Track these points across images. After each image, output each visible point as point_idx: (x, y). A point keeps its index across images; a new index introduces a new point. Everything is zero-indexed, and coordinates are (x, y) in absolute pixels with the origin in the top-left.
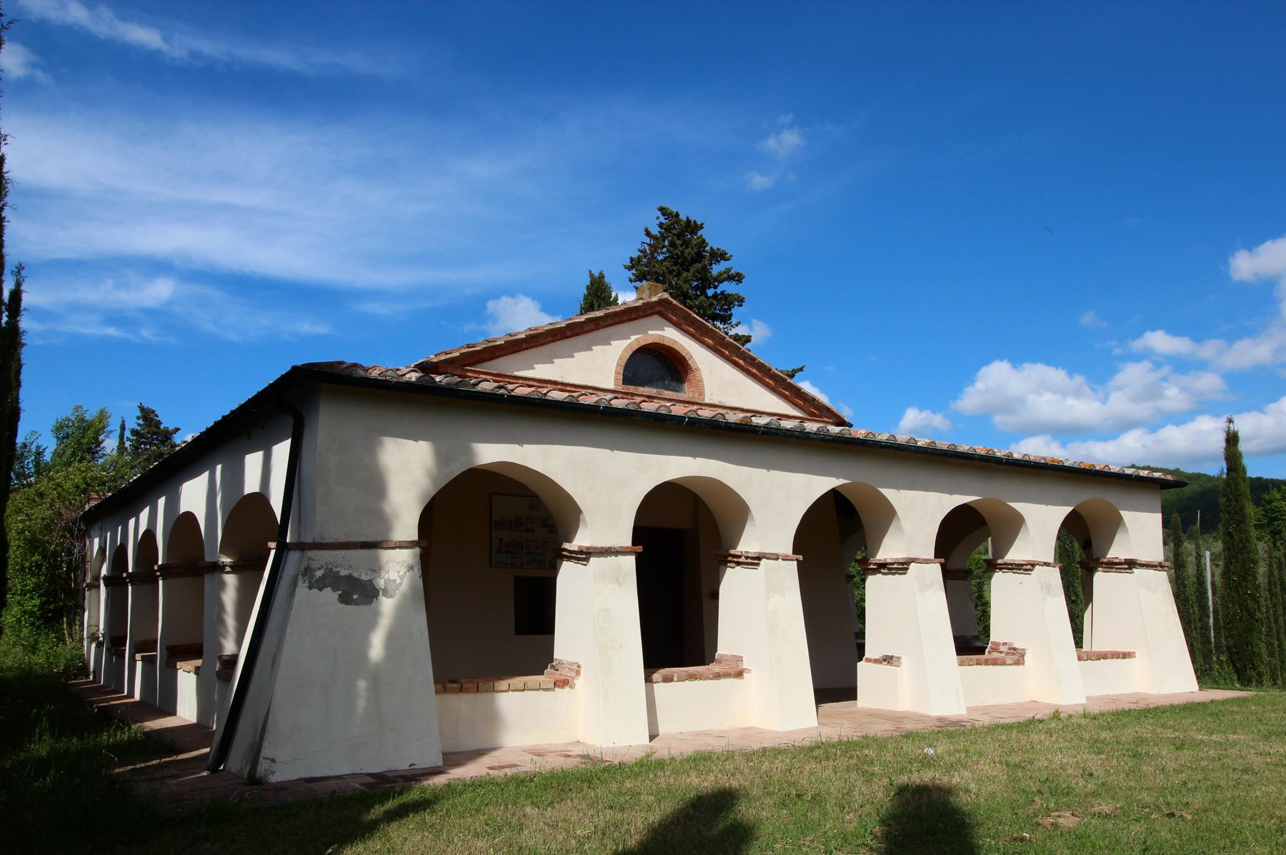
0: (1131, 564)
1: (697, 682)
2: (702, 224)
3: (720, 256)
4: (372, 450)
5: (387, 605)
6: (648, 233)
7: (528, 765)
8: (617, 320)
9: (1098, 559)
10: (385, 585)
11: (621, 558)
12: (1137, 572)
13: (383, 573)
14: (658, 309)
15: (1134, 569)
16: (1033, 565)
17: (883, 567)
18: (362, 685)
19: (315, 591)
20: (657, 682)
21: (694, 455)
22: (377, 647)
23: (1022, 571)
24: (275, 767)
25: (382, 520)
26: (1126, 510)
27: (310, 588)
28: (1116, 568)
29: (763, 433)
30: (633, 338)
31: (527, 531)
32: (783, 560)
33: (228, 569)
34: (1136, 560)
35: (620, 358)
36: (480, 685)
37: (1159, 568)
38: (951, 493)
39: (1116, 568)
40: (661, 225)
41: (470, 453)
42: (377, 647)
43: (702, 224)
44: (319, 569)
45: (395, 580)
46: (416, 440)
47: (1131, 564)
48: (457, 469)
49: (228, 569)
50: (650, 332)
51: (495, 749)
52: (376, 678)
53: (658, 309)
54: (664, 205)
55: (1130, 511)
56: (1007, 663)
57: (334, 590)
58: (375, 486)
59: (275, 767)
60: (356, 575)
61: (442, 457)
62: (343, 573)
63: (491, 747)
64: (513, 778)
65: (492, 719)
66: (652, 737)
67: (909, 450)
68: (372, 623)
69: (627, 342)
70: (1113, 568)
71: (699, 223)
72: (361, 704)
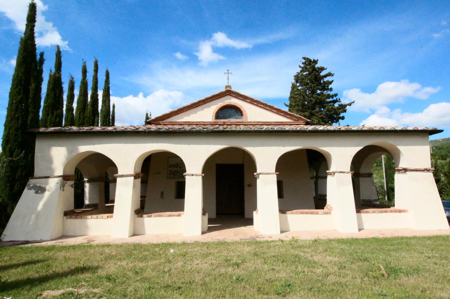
0: (405, 170)
1: (161, 218)
2: (317, 60)
3: (322, 69)
4: (49, 151)
5: (47, 194)
6: (300, 67)
7: (155, 241)
8: (212, 99)
9: (394, 168)
10: (49, 188)
11: (128, 178)
12: (408, 173)
13: (49, 185)
14: (227, 93)
15: (407, 172)
16: (334, 173)
17: (399, 170)
18: (34, 216)
19: (29, 190)
20: (145, 217)
21: (157, 143)
22: (40, 207)
23: (400, 173)
24: (5, 237)
25: (52, 170)
26: (402, 145)
27: (28, 189)
28: (401, 172)
29: (195, 132)
30: (219, 104)
31: (180, 167)
32: (195, 176)
33: (86, 182)
34: (407, 168)
35: (214, 111)
36: (82, 217)
37: (425, 171)
38: (284, 146)
39: (401, 172)
40: (303, 63)
41: (77, 149)
42: (40, 207)
43: (317, 60)
44: (32, 184)
45: (52, 187)
46: (62, 147)
47: (405, 170)
48: (74, 154)
49: (86, 182)
50: (225, 101)
51: (289, 231)
52: (38, 215)
53: (227, 93)
54: (304, 57)
55: (404, 146)
56: (319, 213)
57: (34, 190)
58: (50, 161)
59: (5, 237)
60: (41, 186)
61: (69, 152)
62: (38, 185)
63: (137, 234)
64: (89, 245)
65: (86, 227)
66: (360, 230)
67: (251, 132)
68: (41, 199)
69: (217, 106)
70: (400, 172)
71: (316, 59)
72: (31, 222)
